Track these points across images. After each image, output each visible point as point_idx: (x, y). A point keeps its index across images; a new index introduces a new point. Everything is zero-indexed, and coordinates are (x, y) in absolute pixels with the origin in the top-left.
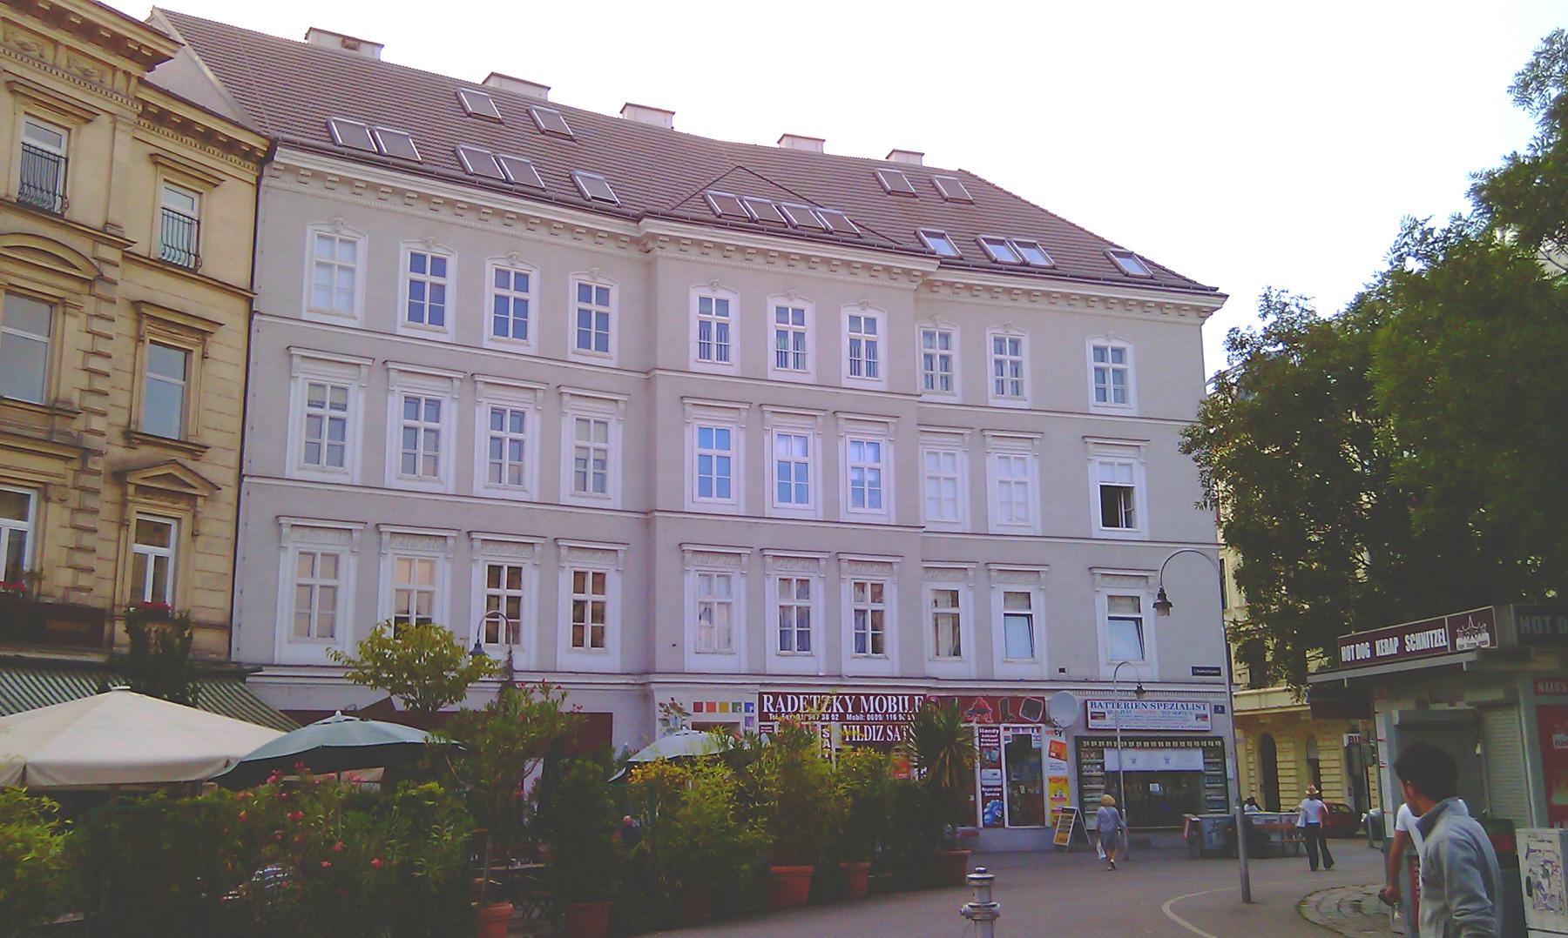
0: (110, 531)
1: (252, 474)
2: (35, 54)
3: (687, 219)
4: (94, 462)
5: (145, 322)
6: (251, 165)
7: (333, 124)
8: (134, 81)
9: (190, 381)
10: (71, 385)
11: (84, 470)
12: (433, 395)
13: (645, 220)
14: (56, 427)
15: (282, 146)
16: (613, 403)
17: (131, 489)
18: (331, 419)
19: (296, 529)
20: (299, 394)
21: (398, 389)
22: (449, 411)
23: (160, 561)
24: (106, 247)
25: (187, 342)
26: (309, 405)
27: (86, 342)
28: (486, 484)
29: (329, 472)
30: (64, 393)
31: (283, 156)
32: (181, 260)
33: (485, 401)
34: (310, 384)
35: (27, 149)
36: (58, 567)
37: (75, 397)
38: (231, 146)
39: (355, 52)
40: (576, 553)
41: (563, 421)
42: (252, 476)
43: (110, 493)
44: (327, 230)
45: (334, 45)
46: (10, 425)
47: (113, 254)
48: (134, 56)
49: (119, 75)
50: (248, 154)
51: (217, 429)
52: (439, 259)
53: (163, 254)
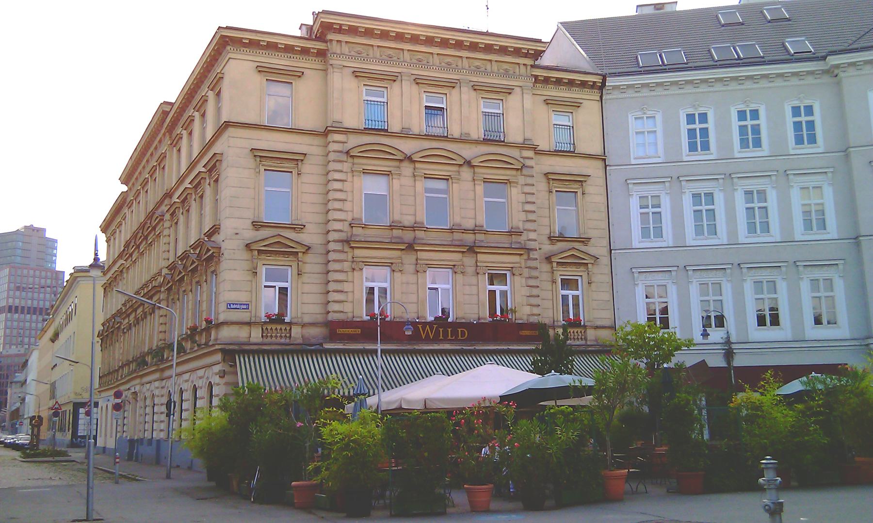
0: (548, 286)
1: (615, 248)
2: (483, 69)
3: (692, 68)
4: (533, 254)
5: (551, 182)
6: (596, 91)
7: (712, 50)
8: (529, 67)
9: (578, 207)
10: (517, 219)
11: (529, 259)
12: (707, 190)
13: (828, 57)
14: (513, 241)
15: (609, 77)
16: (716, 181)
17: (555, 264)
18: (706, 210)
19: (641, 274)
20: (634, 203)
21: (635, 194)
22: (719, 197)
23: (576, 298)
24: (526, 151)
25: (575, 187)
26: (640, 208)
27: (522, 198)
28: (746, 236)
29: (656, 242)
30: (515, 224)
31: (610, 82)
32: (566, 148)
33: (740, 188)
34: (640, 197)
35: (486, 114)
36: (522, 305)
37: (521, 225)
38: (583, 84)
39: (662, 11)
40: (809, 269)
41: (736, 193)
42: (615, 250)
43: (546, 267)
44: (639, 114)
45: (650, 11)
46: (492, 243)
47: (530, 154)
48: (526, 55)
49: (522, 67)
50: (593, 86)
51: (595, 229)
52: (754, 110)
53: (556, 147)
